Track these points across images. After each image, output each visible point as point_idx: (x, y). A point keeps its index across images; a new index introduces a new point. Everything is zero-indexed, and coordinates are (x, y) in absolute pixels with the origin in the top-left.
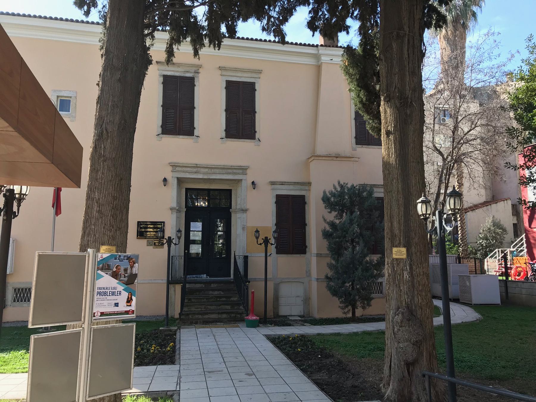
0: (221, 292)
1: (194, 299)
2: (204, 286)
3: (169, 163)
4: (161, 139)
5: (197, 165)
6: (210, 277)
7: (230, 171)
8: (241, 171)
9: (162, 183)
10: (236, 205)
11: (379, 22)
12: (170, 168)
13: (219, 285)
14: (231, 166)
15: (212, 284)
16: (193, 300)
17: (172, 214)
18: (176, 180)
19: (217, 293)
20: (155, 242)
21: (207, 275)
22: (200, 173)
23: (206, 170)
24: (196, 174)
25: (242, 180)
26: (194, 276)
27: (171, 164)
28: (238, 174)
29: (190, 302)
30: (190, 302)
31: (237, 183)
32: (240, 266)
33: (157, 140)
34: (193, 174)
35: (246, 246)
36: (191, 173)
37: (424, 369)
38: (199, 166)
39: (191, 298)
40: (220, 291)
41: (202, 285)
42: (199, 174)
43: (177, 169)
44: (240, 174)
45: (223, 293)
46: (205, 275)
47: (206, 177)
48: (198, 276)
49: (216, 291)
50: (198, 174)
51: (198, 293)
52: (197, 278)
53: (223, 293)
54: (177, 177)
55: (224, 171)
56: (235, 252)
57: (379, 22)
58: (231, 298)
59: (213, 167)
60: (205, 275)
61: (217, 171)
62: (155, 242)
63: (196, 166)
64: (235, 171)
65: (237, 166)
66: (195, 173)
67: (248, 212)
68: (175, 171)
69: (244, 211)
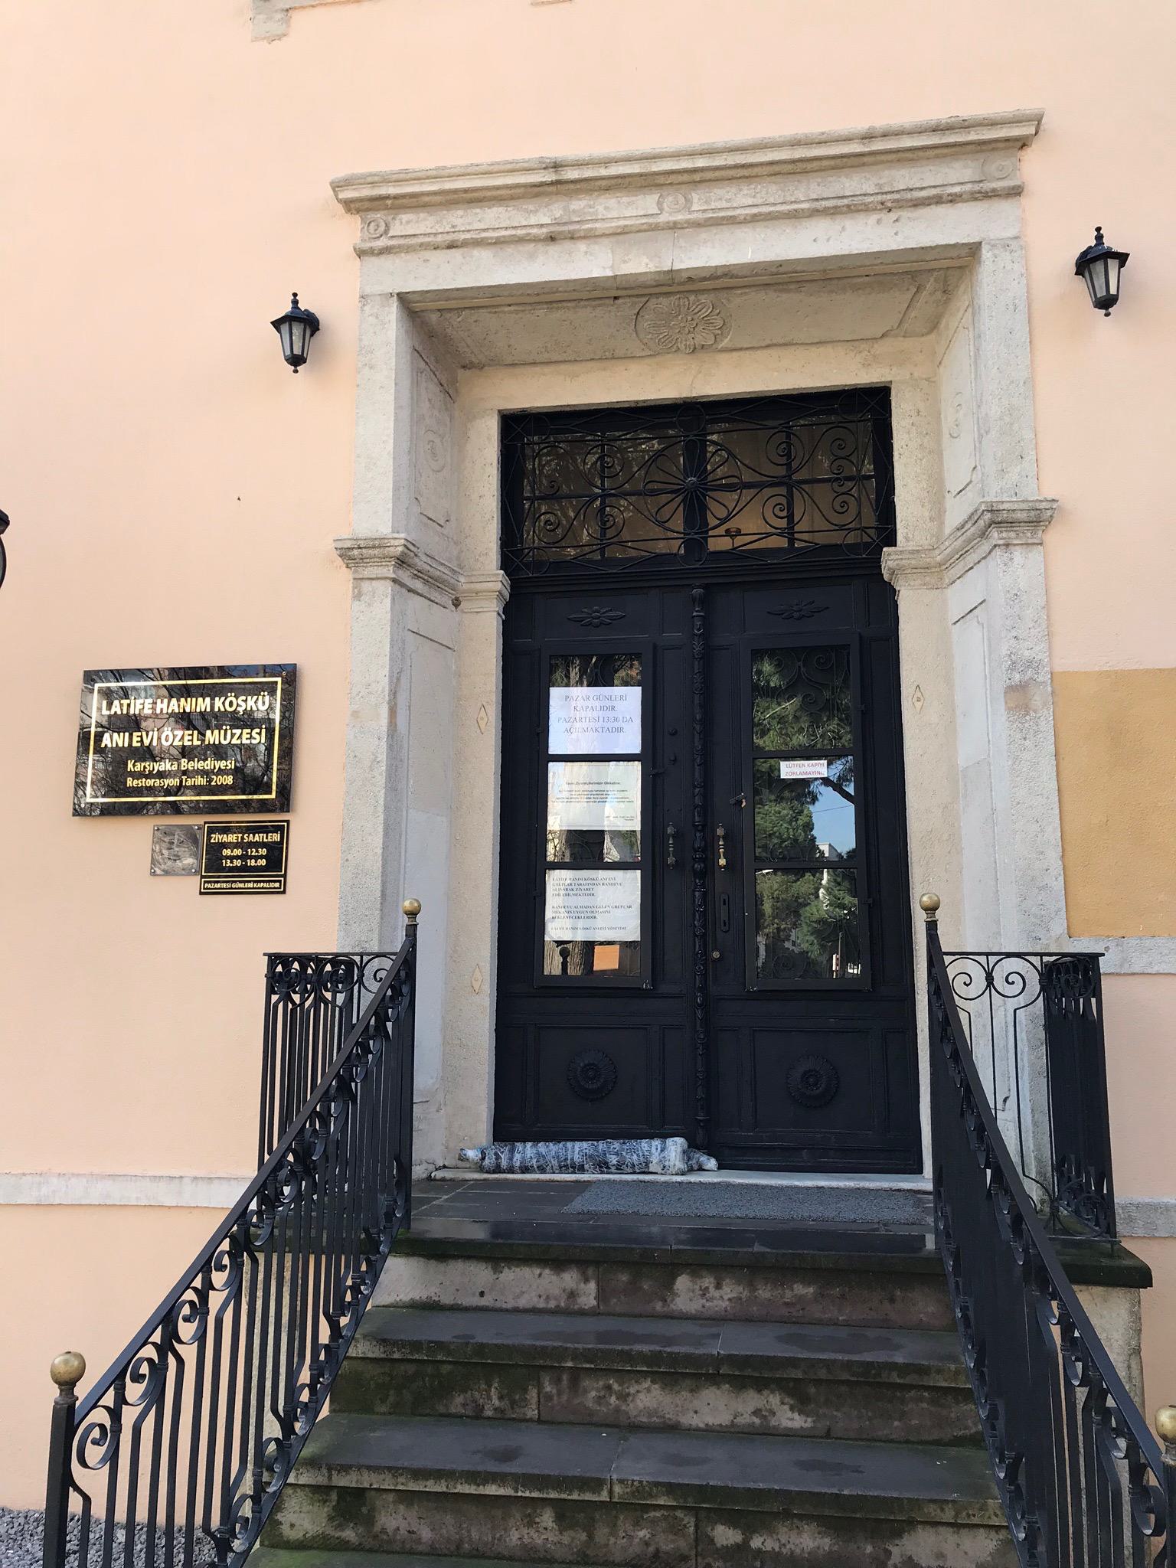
0: (774, 1400)
1: (408, 1498)
2: (588, 1295)
3: (337, 186)
4: (287, 21)
5: (556, 166)
6: (721, 1167)
7: (853, 184)
8: (958, 174)
9: (274, 344)
10: (938, 514)
11: (1093, 1413)
12: (350, 231)
13: (764, 1293)
14: (868, 137)
15: (682, 1282)
16: (393, 1520)
17: (358, 596)
18: (392, 312)
19: (723, 1418)
20: (216, 838)
21: (693, 1145)
22: (590, 236)
23: (643, 206)
24: (554, 249)
25: (973, 251)
26: (577, 1150)
27: (348, 194)
28: (938, 200)
29: (349, 1534)
30: (349, 1534)
31: (933, 325)
32: (1006, 1066)
33: (256, 39)
34: (532, 257)
35: (1056, 866)
36: (510, 250)
37: (599, 436)
38: (572, 174)
39: (367, 1480)
40: (761, 1384)
41: (570, 1278)
42: (582, 246)
43: (407, 224)
44: (953, 199)
45: (795, 1421)
46: (676, 1146)
47: (639, 263)
48: (613, 1149)
49: (715, 1379)
50: (568, 245)
51: (493, 1401)
52: (602, 1166)
53: (795, 1421)
54: (403, 299)
55: (804, 192)
56: (413, 914)
57: (1093, 1413)
58: (911, 1524)
59: (701, 163)
60: (676, 1146)
61: (741, 198)
62: (216, 838)
63: (549, 177)
64: (903, 178)
65: (920, 131)
66: (552, 238)
67: (1052, 537)
68: (383, 242)
69: (1009, 524)
